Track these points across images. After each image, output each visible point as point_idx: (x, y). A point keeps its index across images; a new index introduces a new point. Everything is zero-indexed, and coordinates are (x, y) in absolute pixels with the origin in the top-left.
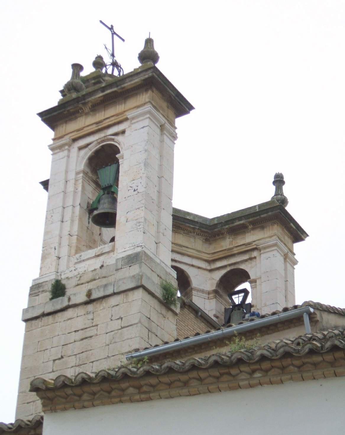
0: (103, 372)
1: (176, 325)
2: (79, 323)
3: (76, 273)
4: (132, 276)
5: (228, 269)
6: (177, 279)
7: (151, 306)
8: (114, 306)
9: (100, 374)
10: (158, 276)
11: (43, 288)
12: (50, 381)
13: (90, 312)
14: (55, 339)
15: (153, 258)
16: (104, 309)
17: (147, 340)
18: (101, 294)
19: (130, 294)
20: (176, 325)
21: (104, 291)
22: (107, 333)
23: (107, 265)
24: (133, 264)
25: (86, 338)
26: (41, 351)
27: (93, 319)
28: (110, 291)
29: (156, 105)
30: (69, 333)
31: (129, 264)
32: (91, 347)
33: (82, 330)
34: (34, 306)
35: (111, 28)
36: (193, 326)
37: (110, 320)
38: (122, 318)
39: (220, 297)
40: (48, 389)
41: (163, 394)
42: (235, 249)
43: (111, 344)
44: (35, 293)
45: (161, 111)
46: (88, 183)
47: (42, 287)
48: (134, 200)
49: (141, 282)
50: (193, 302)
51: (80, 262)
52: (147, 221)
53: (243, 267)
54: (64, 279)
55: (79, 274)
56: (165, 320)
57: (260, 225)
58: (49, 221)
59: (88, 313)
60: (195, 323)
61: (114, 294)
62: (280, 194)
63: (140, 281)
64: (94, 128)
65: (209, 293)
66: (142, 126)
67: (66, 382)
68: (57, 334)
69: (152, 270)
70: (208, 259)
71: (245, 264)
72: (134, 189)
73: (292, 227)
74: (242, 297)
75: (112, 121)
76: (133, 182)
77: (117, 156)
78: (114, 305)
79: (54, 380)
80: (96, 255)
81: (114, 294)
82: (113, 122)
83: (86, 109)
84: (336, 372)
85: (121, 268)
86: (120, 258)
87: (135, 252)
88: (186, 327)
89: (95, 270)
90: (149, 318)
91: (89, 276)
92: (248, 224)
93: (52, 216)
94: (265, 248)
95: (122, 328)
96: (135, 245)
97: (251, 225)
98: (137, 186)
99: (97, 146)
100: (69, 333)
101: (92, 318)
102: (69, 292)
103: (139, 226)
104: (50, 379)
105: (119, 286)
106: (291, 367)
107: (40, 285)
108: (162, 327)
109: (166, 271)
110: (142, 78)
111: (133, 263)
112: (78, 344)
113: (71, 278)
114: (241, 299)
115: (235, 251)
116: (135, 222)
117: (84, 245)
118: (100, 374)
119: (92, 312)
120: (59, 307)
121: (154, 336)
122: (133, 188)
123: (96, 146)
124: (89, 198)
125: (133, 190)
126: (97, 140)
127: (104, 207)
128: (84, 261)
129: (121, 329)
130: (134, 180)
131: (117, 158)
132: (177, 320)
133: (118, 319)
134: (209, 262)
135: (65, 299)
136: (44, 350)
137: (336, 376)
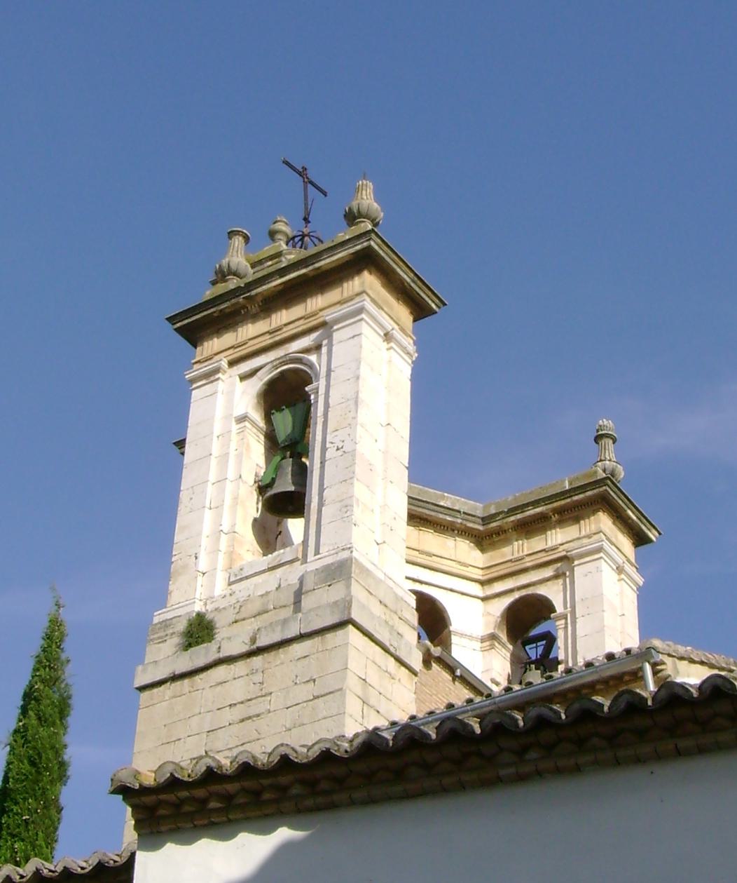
0: (246, 755)
1: (415, 693)
2: (238, 690)
3: (233, 600)
4: (333, 603)
5: (517, 595)
6: (417, 610)
7: (367, 658)
8: (299, 659)
9: (239, 757)
10: (381, 602)
11: (173, 628)
12: (149, 773)
13: (257, 670)
14: (195, 720)
15: (372, 570)
16: (282, 663)
17: (360, 720)
18: (276, 637)
19: (329, 636)
20: (415, 693)
21: (282, 630)
22: (287, 708)
23: (289, 585)
24: (334, 581)
25: (249, 718)
26: (168, 743)
27: (262, 683)
28: (293, 631)
29: (376, 299)
30: (219, 709)
31: (327, 582)
32: (259, 733)
33: (242, 703)
34: (156, 662)
35: (302, 173)
36: (446, 695)
37: (293, 684)
38: (314, 681)
39: (503, 647)
40: (144, 790)
41: (357, 795)
42: (528, 559)
43: (295, 727)
44: (159, 638)
45: (385, 309)
46: (257, 438)
47: (172, 626)
48: (337, 466)
49: (350, 613)
50: (452, 657)
51: (241, 580)
52: (360, 503)
53: (542, 591)
54: (212, 611)
55: (238, 602)
56: (394, 683)
57: (571, 515)
58: (186, 507)
59: (254, 671)
60: (450, 689)
61: (302, 637)
62: (608, 458)
63: (346, 612)
64: (268, 340)
65: (482, 640)
66: (352, 335)
67: (176, 775)
68: (197, 711)
69: (369, 592)
70: (481, 578)
71: (546, 586)
72: (338, 447)
73: (630, 518)
74: (543, 647)
75: (298, 327)
76: (336, 433)
77: (307, 389)
78: (299, 657)
79: (155, 772)
80: (270, 566)
81: (302, 637)
82: (300, 329)
83: (253, 307)
84: (678, 747)
85: (314, 589)
86: (312, 571)
87: (338, 559)
88: (435, 697)
89: (267, 593)
90: (364, 680)
91: (256, 606)
92: (551, 514)
93: (191, 499)
94: (581, 556)
95: (316, 698)
96: (338, 547)
97: (556, 515)
98: (343, 441)
99: (273, 371)
100: (219, 709)
101: (261, 681)
102: (221, 633)
103: (346, 512)
104: (149, 771)
105: (310, 622)
106: (595, 741)
107: (168, 622)
108: (388, 696)
109: (396, 595)
110: (352, 251)
111: (334, 579)
112: (235, 728)
113: (224, 608)
114: (540, 650)
115: (528, 563)
116: (338, 505)
117: (248, 550)
118: (239, 757)
119: (261, 670)
120: (201, 662)
121: (374, 713)
122: (336, 445)
123: (271, 373)
124: (257, 465)
125: (336, 448)
126: (271, 362)
127: (286, 485)
128: (247, 578)
129: (313, 700)
130: (337, 430)
131: (307, 392)
132: (416, 683)
133: (308, 681)
134: (483, 583)
135: (213, 646)
136: (175, 741)
137: (680, 755)
